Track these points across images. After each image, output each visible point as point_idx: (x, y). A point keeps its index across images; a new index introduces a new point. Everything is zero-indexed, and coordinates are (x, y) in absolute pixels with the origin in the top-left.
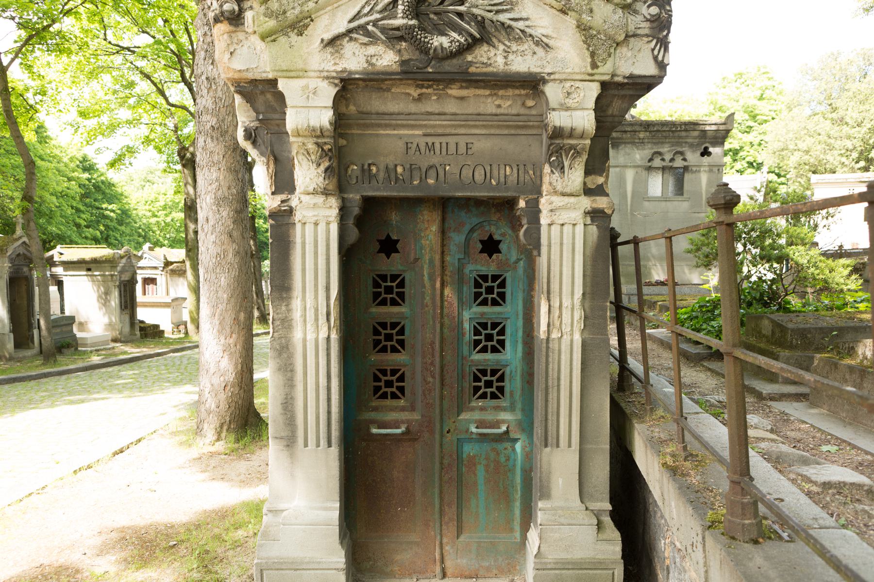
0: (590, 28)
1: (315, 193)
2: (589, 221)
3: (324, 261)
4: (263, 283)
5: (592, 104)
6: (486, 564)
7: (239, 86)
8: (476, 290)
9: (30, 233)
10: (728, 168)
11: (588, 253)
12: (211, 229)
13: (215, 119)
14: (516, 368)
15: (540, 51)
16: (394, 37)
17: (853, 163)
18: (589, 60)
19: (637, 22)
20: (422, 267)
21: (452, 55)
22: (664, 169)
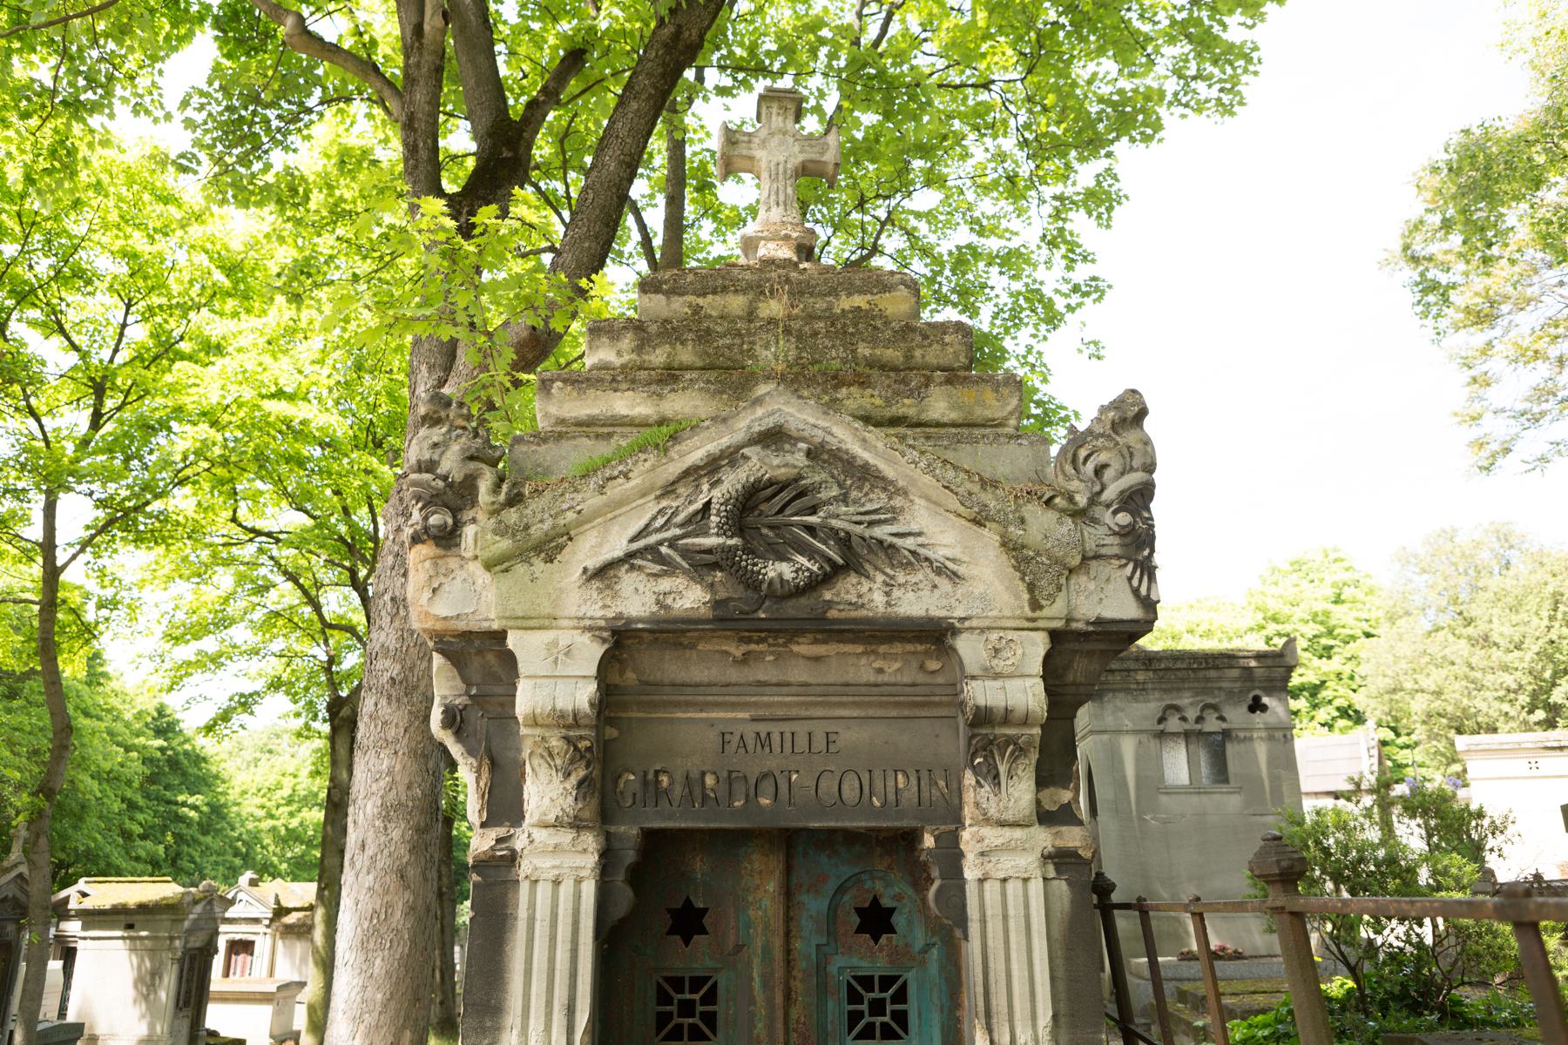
0: (1023, 547)
1: (558, 824)
2: (1052, 873)
3: (568, 955)
4: (457, 949)
5: (1037, 667)
7: (441, 641)
8: (852, 1007)
9: (34, 857)
10: (1305, 721)
11: (1056, 934)
12: (367, 863)
13: (398, 667)
15: (944, 584)
16: (702, 565)
17: (1524, 714)
18: (1026, 596)
19: (1098, 536)
20: (749, 964)
21: (799, 592)
22: (1187, 735)
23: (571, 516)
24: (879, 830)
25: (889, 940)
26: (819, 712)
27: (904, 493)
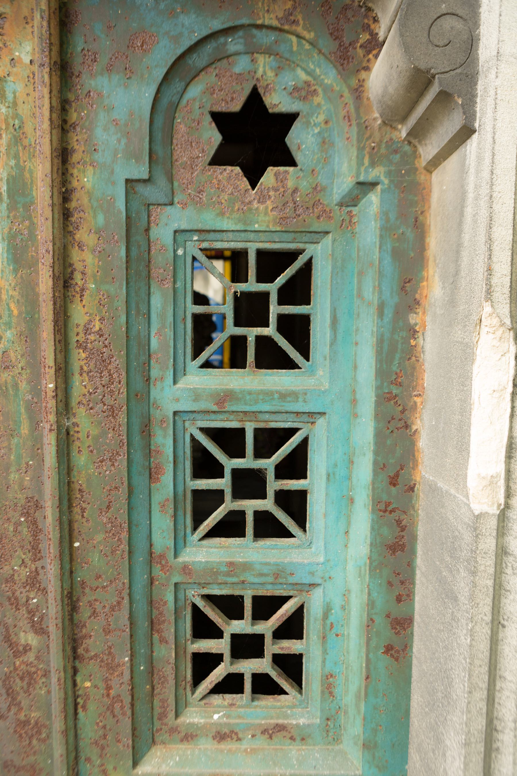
14: (346, 594)
25: (281, 180)
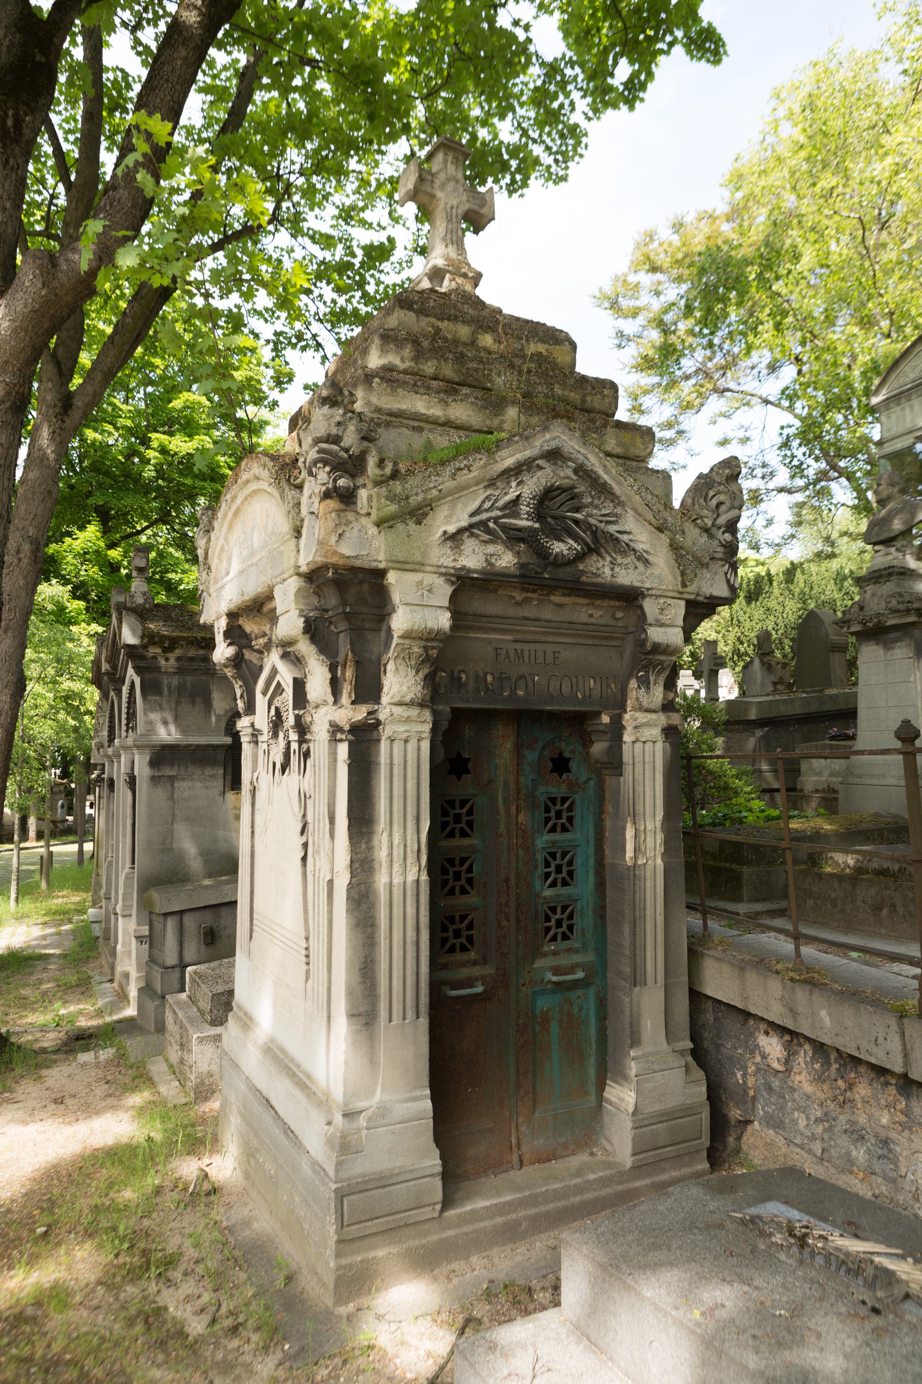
1: (412, 704)
6: (563, 1140)
15: (641, 567)
16: (514, 537)
18: (680, 579)
23: (435, 493)
24: (564, 712)
26: (551, 639)
27: (622, 504)
